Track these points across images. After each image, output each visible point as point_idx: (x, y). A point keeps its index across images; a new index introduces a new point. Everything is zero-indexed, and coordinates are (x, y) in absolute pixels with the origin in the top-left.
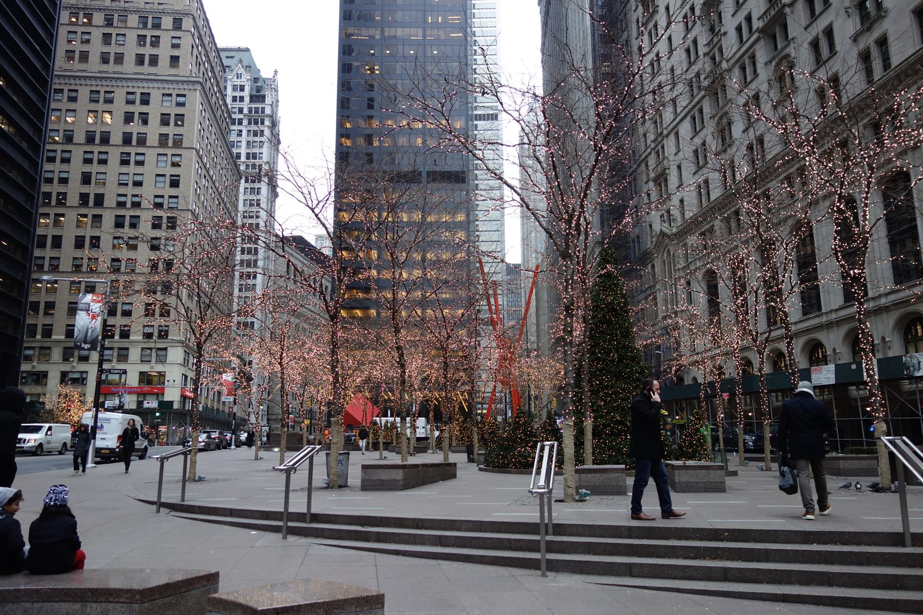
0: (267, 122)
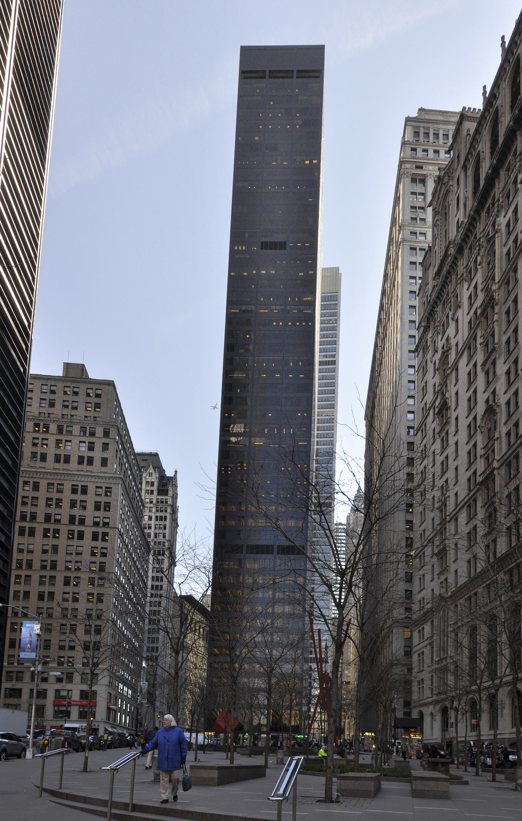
0: (169, 510)
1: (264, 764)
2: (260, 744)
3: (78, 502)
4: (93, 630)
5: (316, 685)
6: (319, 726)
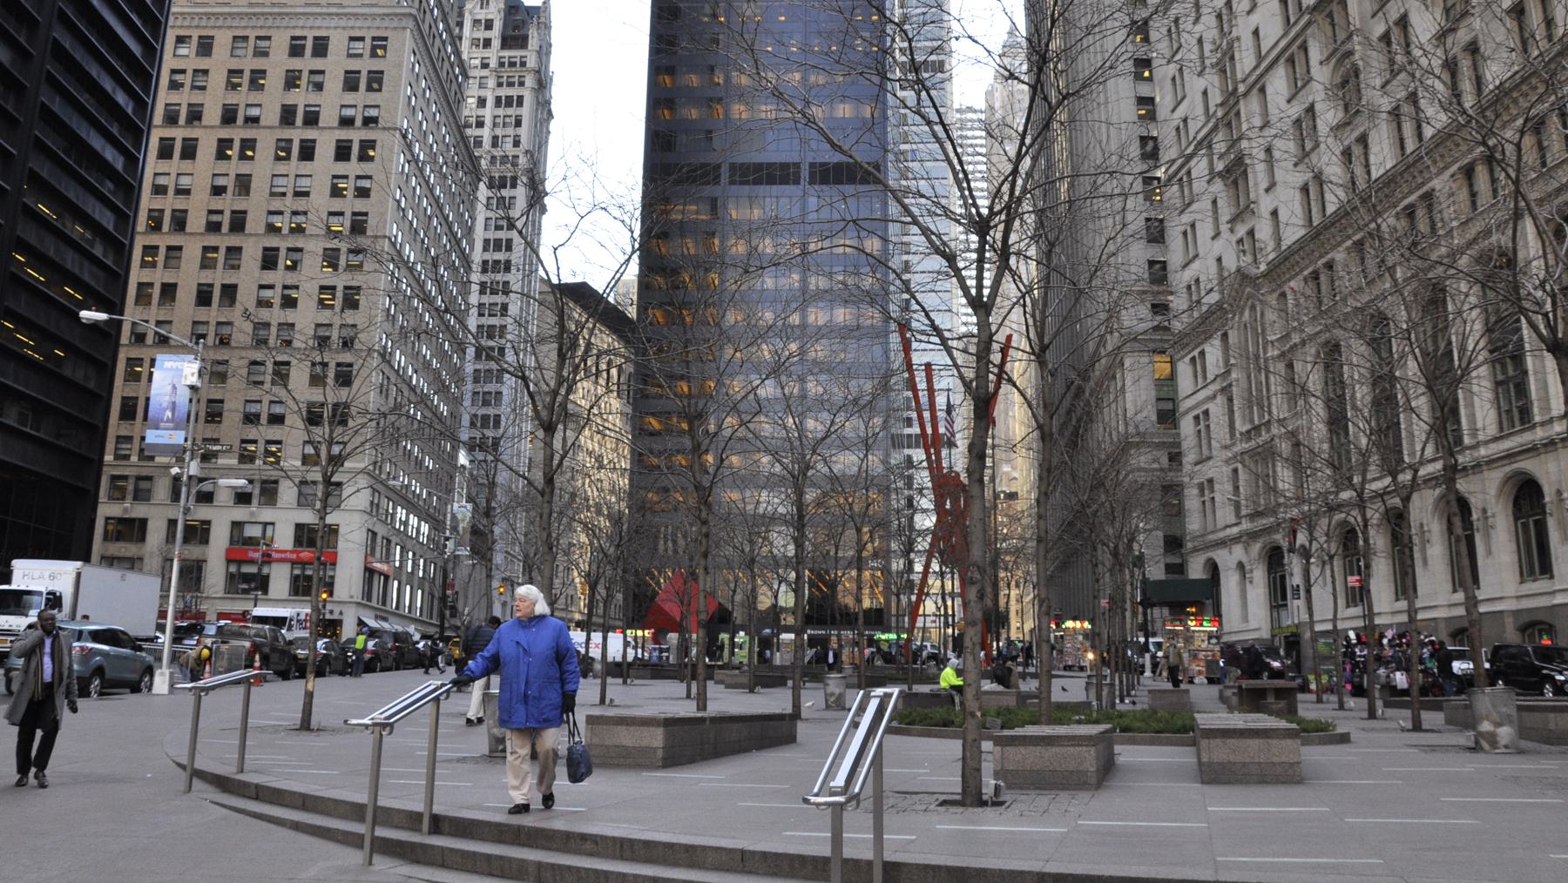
0: (530, 81)
1: (789, 710)
2: (778, 659)
3: (305, 75)
4: (331, 374)
5: (926, 503)
6: (937, 608)
